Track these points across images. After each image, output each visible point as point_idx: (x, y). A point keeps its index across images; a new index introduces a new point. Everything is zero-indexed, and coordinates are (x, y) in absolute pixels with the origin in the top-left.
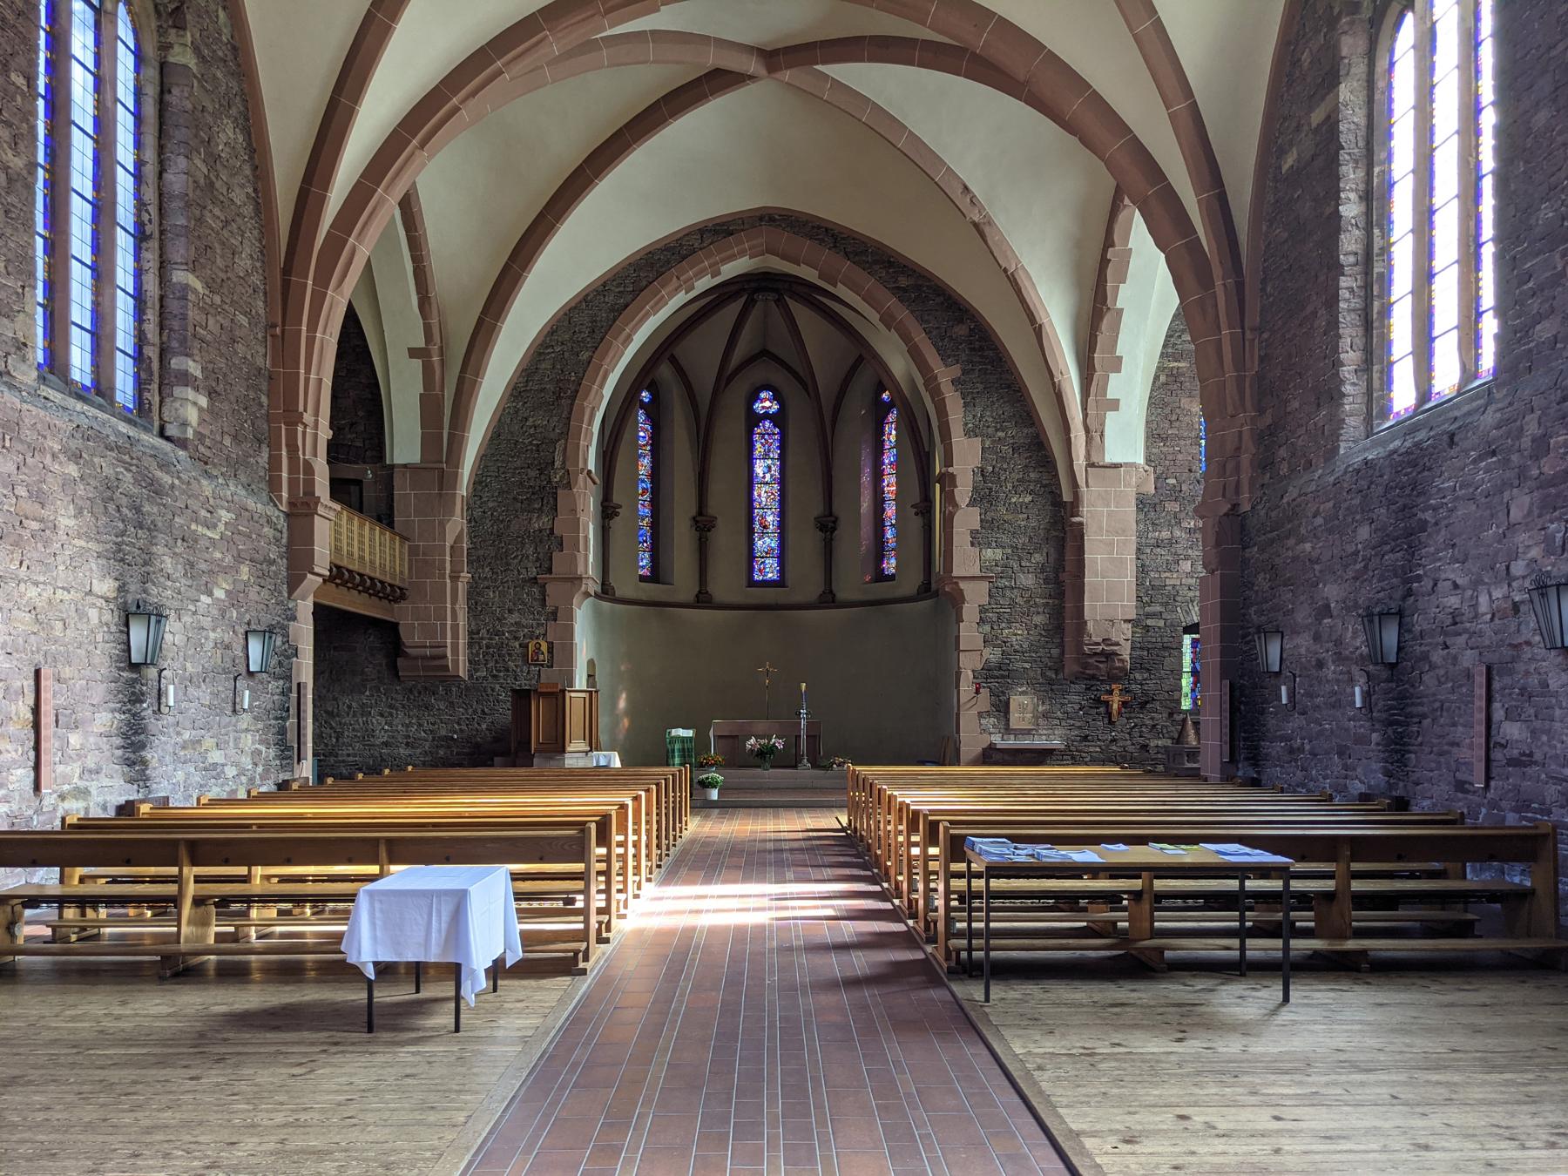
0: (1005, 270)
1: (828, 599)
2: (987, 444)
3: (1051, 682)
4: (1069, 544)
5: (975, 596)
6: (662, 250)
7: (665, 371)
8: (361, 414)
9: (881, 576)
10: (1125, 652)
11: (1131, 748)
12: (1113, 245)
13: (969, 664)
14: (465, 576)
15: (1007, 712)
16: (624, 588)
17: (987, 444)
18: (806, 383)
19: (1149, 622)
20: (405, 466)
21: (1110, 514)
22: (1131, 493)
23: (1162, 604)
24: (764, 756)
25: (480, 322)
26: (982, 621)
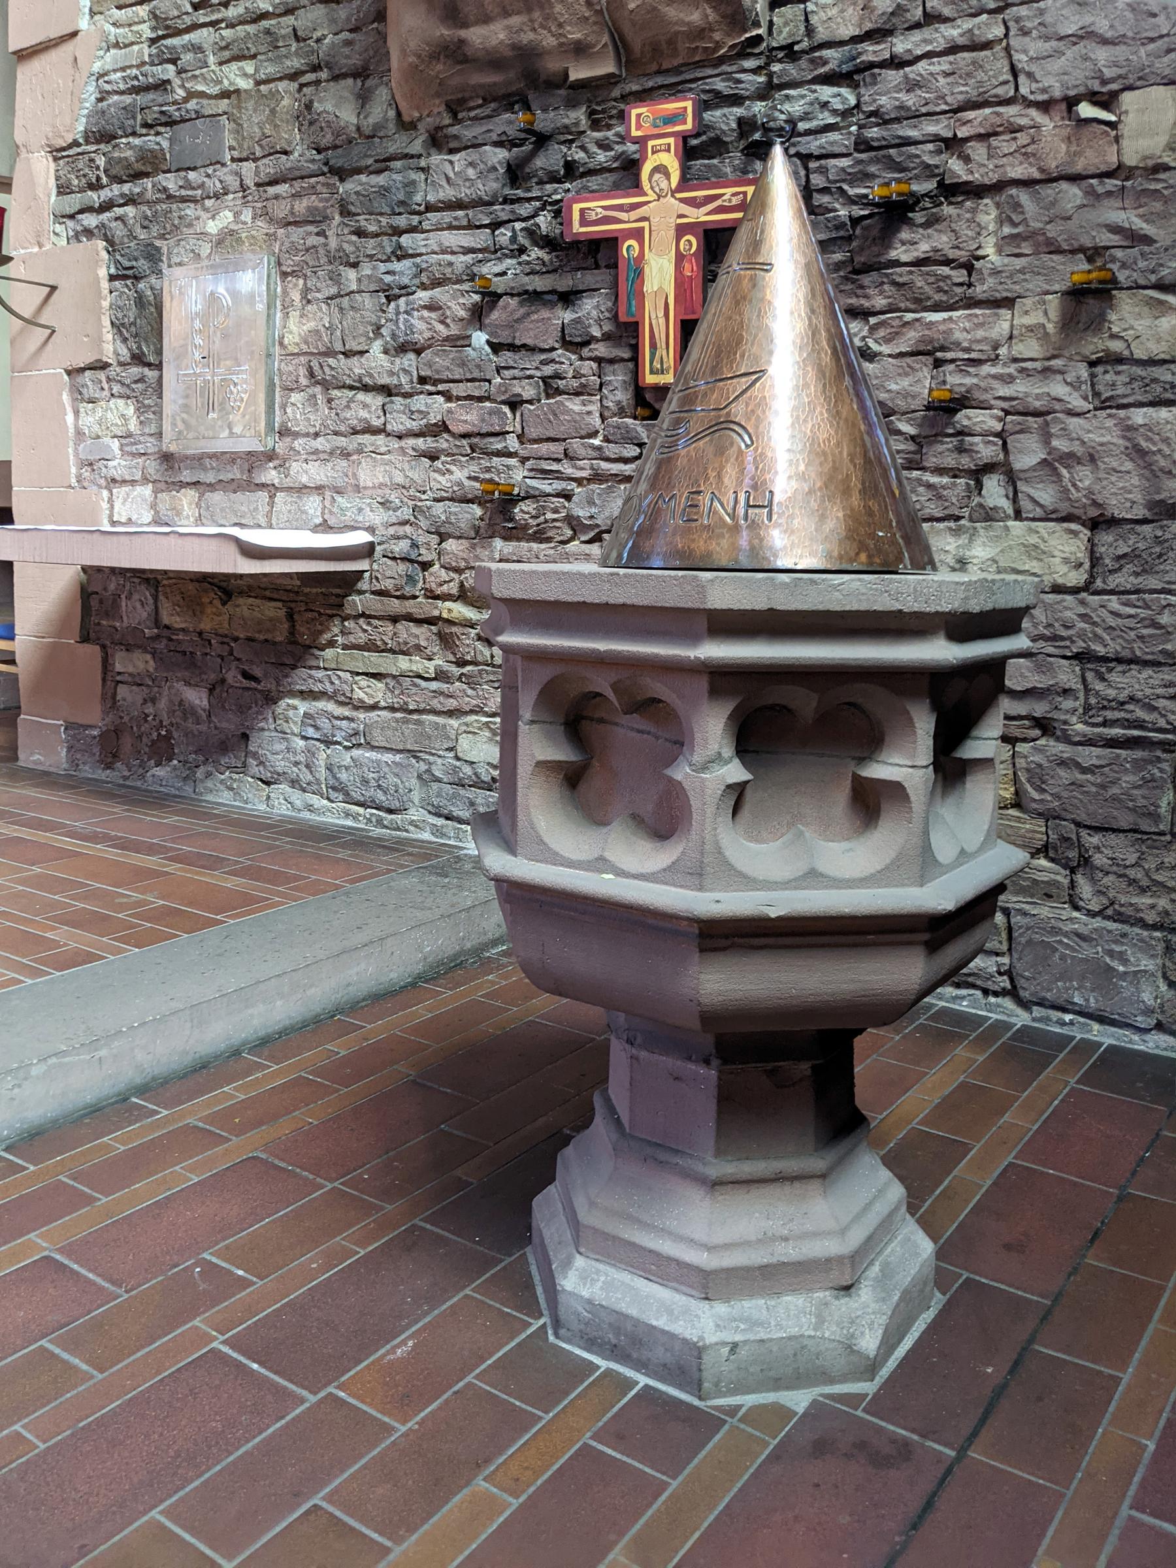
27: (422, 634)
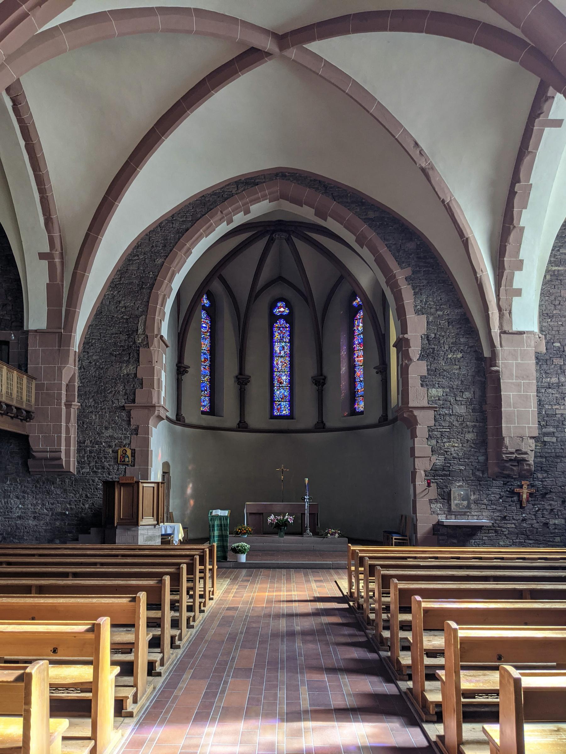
0: (443, 201)
1: (320, 427)
2: (431, 319)
3: (479, 480)
4: (490, 386)
5: (425, 420)
6: (211, 195)
7: (217, 286)
8: (10, 298)
9: (354, 412)
10: (531, 459)
11: (536, 525)
12: (519, 182)
13: (422, 466)
14: (76, 404)
15: (449, 499)
16: (191, 417)
17: (431, 319)
18: (307, 297)
19: (546, 439)
20: (36, 331)
21: (518, 365)
22: (531, 351)
23: (554, 427)
24: (280, 528)
25: (87, 236)
26: (430, 437)
27: (493, 531)
